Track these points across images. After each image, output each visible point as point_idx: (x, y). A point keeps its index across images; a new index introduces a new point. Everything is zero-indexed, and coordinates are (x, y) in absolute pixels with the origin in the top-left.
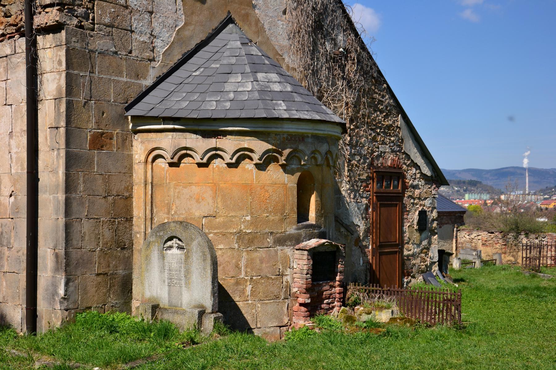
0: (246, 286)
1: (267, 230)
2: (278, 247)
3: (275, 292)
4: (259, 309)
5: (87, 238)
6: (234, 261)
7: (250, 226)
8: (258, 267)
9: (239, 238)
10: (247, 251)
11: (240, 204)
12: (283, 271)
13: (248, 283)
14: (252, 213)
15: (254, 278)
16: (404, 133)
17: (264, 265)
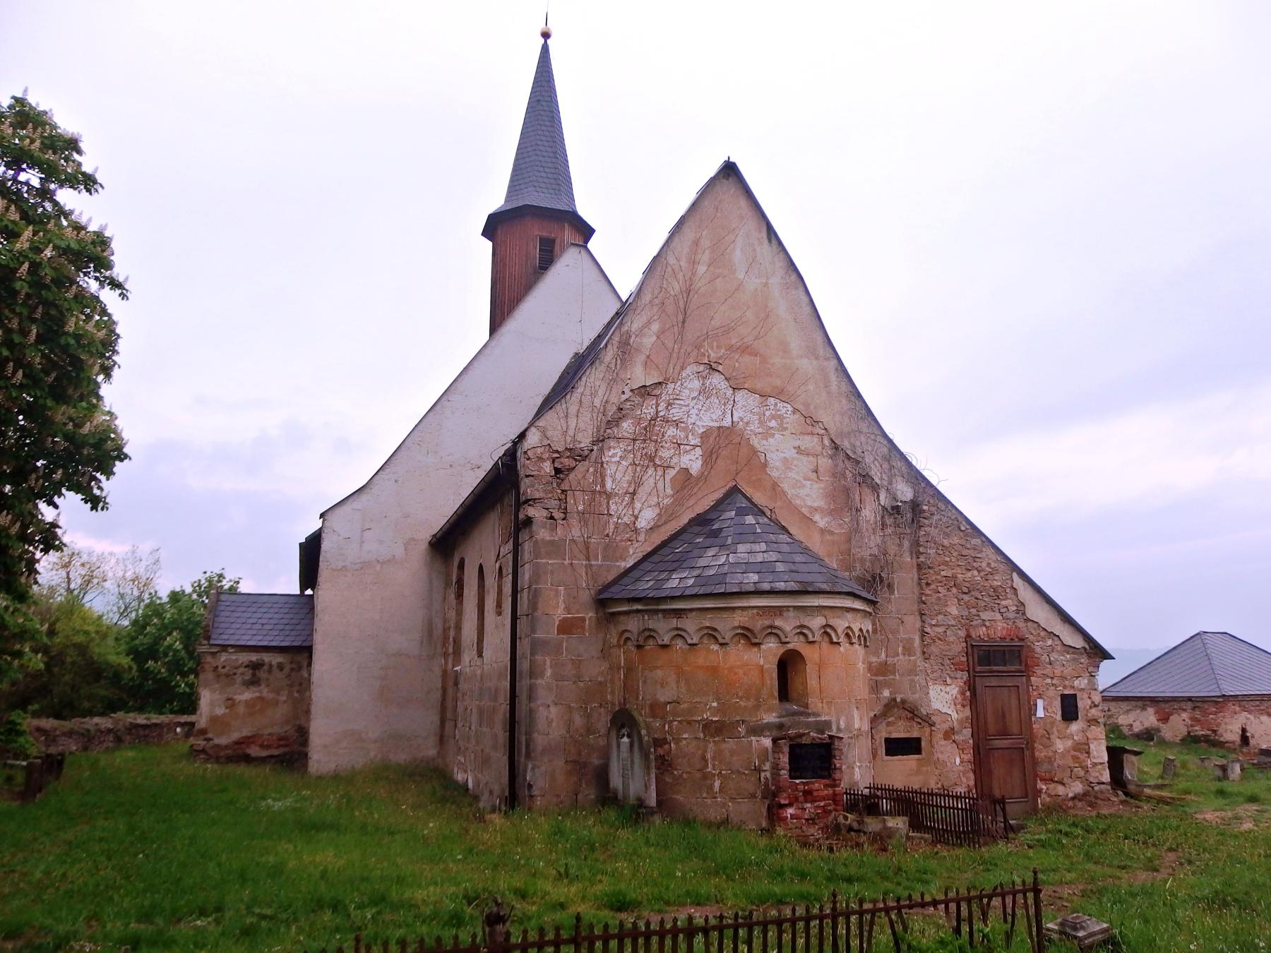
14: (718, 699)
16: (1025, 594)
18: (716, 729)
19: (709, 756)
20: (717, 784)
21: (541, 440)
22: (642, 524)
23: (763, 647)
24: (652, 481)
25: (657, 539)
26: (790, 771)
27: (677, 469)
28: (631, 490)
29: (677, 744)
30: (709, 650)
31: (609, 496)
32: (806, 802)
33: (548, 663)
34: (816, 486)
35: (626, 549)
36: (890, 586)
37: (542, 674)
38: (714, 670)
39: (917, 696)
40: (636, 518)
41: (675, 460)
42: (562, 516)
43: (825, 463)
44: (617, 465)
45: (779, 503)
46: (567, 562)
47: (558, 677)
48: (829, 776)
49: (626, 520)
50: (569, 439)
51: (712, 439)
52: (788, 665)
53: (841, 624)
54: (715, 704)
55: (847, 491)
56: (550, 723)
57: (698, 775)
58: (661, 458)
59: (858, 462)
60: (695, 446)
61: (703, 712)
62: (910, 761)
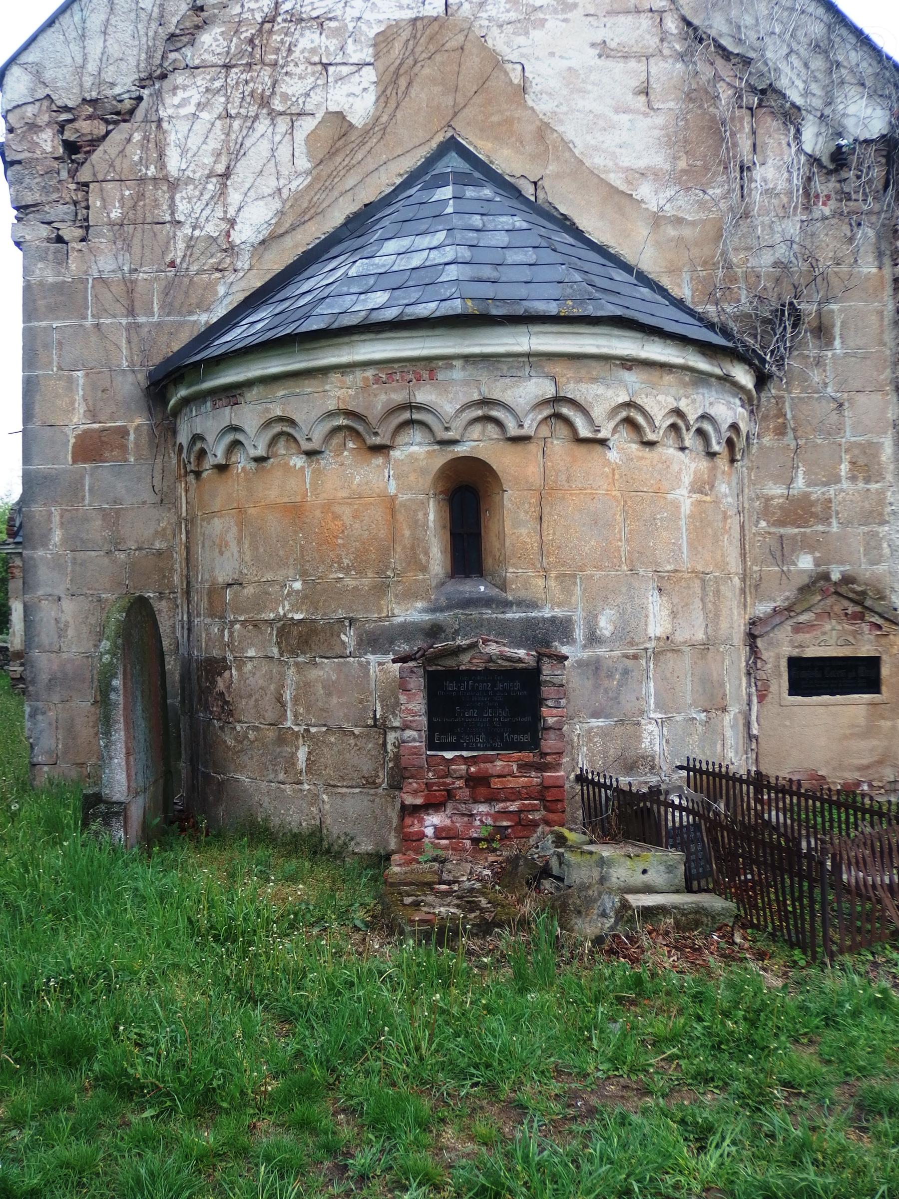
0: (297, 749)
1: (341, 614)
2: (370, 657)
3: (365, 768)
4: (327, 807)
5: (71, 632)
6: (272, 687)
7: (303, 603)
8: (320, 704)
9: (281, 633)
10: (297, 664)
11: (281, 553)
12: (384, 718)
13: (301, 741)
14: (304, 574)
15: (313, 730)
17: (334, 700)
18: (302, 639)
19: (288, 696)
20: (302, 754)
21: (33, 90)
22: (245, 233)
23: (395, 454)
24: (264, 147)
25: (277, 261)
26: (432, 727)
27: (319, 116)
28: (220, 168)
29: (239, 669)
30: (288, 469)
31: (174, 185)
32: (476, 801)
33: (56, 519)
34: (644, 123)
35: (210, 287)
36: (822, 332)
37: (44, 540)
38: (295, 511)
39: (882, 568)
40: (232, 223)
41: (316, 97)
42: (79, 233)
43: (666, 71)
44: (189, 124)
45: (552, 168)
46: (89, 322)
47: (75, 544)
48: (534, 744)
49: (212, 229)
50: (88, 81)
51: (398, 46)
52: (467, 494)
53: (602, 396)
54: (298, 585)
55: (718, 130)
56: (61, 632)
57: (271, 734)
58: (285, 97)
59: (747, 62)
60: (361, 65)
61: (278, 602)
62: (851, 707)
